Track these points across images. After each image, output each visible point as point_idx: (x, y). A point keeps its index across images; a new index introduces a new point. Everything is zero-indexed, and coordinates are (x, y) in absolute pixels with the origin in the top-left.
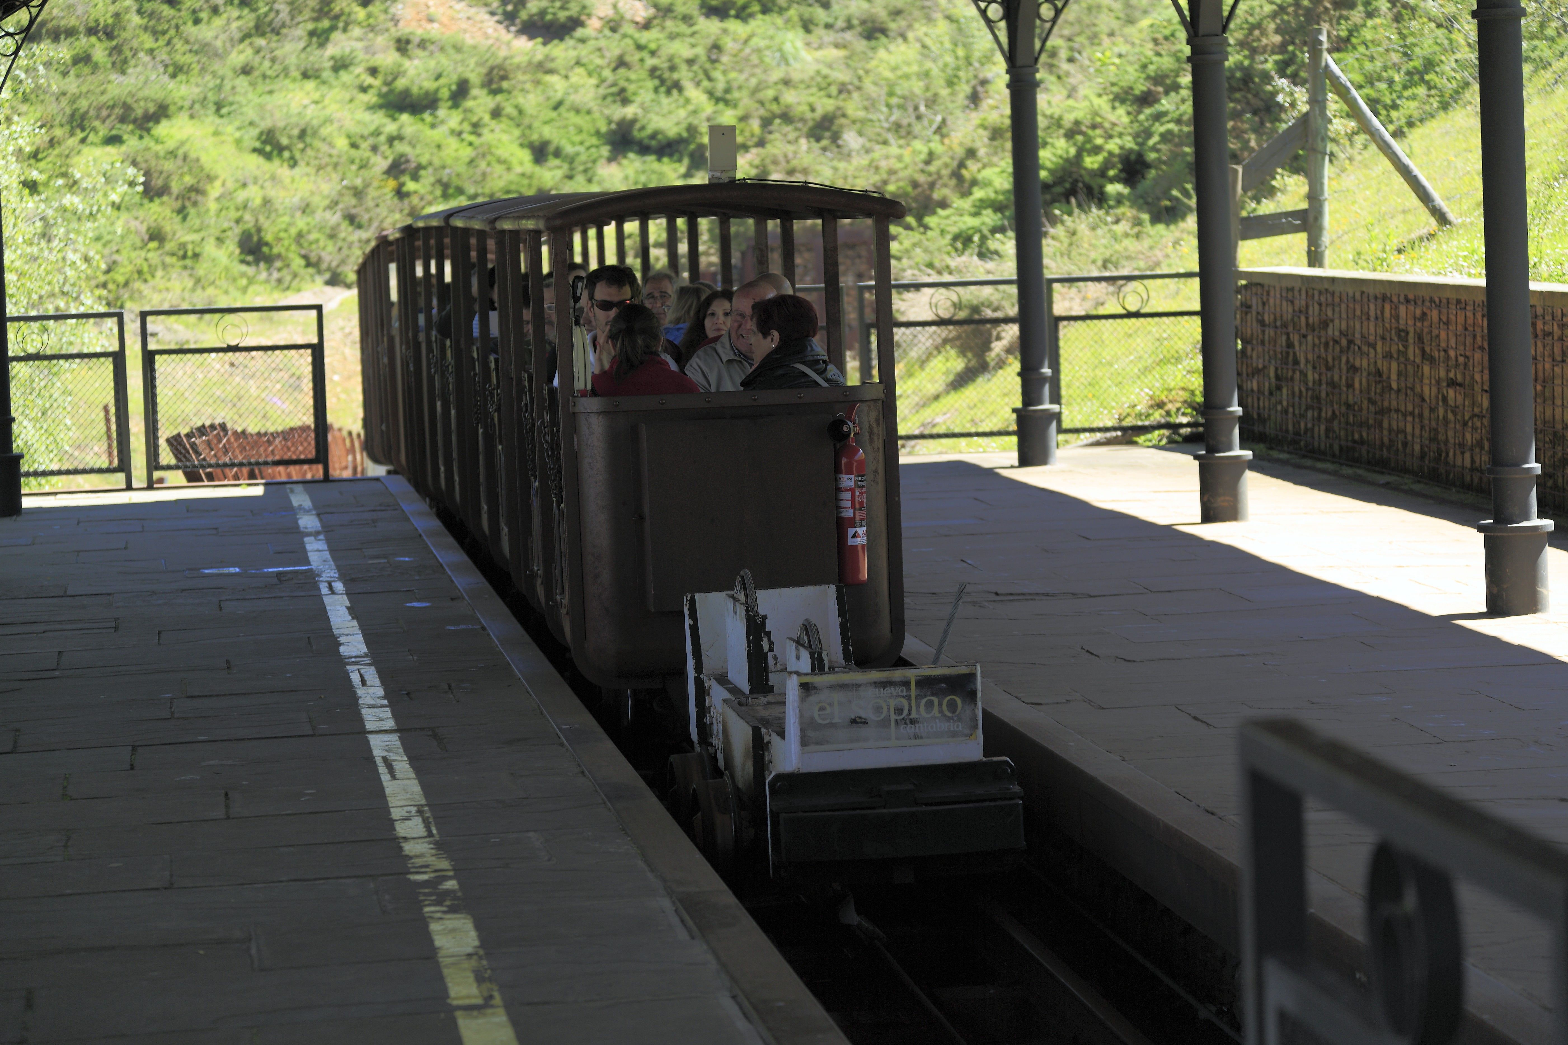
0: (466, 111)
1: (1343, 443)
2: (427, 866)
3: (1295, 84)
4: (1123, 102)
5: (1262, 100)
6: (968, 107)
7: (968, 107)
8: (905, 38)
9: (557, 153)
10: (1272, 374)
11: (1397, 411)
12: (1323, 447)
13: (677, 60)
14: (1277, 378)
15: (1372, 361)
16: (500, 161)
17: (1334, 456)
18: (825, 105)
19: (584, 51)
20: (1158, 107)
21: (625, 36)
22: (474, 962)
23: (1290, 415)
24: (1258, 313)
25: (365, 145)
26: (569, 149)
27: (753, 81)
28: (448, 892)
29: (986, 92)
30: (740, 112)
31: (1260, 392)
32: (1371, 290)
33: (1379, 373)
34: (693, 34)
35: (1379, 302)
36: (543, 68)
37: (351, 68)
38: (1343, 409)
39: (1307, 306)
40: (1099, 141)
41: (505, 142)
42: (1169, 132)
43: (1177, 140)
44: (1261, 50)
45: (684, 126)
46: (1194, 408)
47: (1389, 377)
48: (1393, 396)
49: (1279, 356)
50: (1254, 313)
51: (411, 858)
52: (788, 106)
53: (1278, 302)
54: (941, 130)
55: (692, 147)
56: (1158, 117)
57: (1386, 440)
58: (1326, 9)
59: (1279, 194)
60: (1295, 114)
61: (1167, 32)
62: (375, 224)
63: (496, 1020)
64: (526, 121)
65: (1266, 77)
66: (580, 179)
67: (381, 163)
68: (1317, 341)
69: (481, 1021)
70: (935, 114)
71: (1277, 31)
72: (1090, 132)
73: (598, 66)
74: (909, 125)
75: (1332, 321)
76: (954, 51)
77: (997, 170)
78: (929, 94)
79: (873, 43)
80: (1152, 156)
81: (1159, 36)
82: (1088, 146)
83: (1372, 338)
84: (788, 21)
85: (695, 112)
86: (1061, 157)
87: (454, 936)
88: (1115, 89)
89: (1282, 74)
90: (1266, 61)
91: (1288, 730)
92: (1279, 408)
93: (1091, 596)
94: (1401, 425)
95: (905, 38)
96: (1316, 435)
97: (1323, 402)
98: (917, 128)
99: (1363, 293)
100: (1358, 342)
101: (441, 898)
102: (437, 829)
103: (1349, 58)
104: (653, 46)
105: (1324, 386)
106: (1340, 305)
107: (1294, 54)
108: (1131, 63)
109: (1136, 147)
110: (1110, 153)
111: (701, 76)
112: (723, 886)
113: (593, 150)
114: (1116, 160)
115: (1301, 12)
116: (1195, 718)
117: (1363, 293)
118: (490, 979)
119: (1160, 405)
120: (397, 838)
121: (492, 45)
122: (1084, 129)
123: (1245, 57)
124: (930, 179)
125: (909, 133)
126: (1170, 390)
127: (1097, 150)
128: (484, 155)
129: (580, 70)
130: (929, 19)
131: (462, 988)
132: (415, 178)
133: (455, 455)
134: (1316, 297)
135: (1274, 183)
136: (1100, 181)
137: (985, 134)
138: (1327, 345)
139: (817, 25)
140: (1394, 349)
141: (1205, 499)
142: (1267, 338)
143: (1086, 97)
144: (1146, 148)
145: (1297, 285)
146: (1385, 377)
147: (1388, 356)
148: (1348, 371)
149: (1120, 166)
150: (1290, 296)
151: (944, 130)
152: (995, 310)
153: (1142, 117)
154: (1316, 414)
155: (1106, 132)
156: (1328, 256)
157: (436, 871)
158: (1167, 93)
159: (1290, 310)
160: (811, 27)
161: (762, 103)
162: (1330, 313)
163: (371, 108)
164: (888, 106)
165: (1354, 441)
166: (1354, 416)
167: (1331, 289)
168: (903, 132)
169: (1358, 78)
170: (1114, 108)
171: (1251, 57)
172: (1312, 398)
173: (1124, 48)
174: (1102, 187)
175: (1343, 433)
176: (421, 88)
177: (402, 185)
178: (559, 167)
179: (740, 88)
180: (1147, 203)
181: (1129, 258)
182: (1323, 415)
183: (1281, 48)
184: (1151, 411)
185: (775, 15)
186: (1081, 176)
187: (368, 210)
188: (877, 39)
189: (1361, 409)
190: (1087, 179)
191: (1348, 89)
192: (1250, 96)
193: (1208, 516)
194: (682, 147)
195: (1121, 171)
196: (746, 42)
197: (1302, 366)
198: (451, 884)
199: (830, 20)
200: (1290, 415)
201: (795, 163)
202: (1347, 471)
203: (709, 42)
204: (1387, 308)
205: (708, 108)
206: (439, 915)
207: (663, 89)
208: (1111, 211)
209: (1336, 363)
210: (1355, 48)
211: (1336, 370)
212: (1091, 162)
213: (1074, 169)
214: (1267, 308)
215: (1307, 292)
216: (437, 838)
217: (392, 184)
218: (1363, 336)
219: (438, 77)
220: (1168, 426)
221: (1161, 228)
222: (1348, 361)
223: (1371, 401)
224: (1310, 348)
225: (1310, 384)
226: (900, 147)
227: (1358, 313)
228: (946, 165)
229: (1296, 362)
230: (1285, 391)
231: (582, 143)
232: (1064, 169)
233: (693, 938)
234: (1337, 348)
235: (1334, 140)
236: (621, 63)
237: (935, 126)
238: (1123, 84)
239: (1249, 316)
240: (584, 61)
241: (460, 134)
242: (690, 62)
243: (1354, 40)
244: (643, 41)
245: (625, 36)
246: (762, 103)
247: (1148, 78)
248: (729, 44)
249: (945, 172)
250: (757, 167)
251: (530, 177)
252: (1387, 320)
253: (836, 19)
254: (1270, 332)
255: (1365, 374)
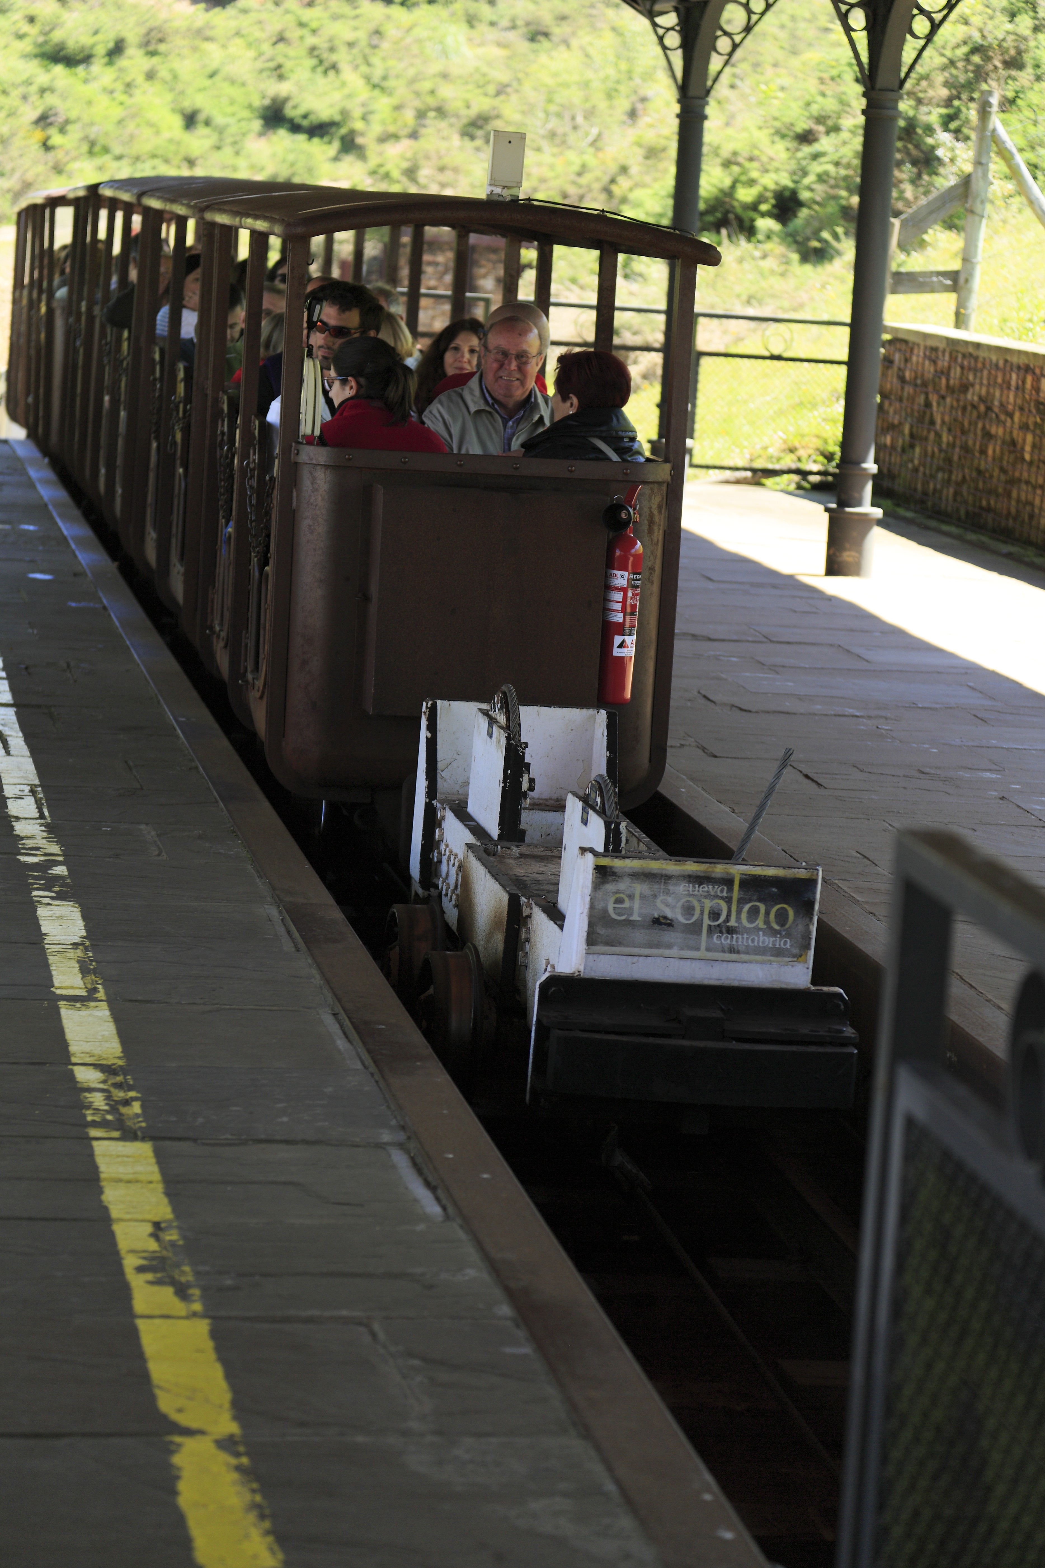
0: (121, 70)
1: (970, 508)
2: (38, 849)
3: (958, 140)
4: (783, 136)
5: (922, 151)
6: (624, 123)
7: (624, 123)
8: (568, 46)
9: (207, 123)
10: (907, 430)
11: (1028, 482)
12: (949, 509)
13: (336, 42)
14: (912, 435)
15: (1008, 430)
16: (151, 125)
17: (959, 519)
18: (481, 104)
19: (244, 22)
20: (816, 147)
21: (287, 12)
22: (79, 953)
23: (920, 475)
24: (899, 369)
25: (16, 93)
26: (219, 119)
27: (411, 72)
28: (57, 878)
29: (645, 109)
30: (394, 101)
31: (893, 447)
32: (1015, 360)
33: (1013, 443)
34: (357, 17)
35: (1022, 373)
36: (202, 35)
37: (9, 14)
38: (974, 474)
39: (949, 368)
40: (754, 174)
41: (159, 109)
42: (826, 173)
43: (832, 182)
44: (926, 101)
45: (337, 108)
46: (826, 457)
47: (1023, 449)
48: (1025, 467)
49: (916, 414)
50: (895, 369)
51: (22, 838)
52: (443, 100)
53: (921, 360)
54: (596, 144)
55: (343, 131)
56: (816, 156)
57: (1013, 510)
58: (996, 67)
59: (929, 248)
60: (954, 169)
61: (834, 72)
62: (17, 175)
63: (99, 1013)
64: (180, 87)
65: (929, 130)
66: (228, 151)
67: (30, 113)
68: (955, 404)
69: (84, 1013)
70: (592, 126)
71: (946, 84)
72: (747, 165)
73: (257, 40)
74: (565, 135)
75: (973, 385)
76: (616, 64)
77: (649, 191)
78: (588, 105)
79: (535, 46)
80: (805, 195)
81: (826, 76)
82: (744, 178)
83: (1010, 407)
84: (453, 14)
85: (350, 96)
86: (715, 186)
87: (61, 924)
88: (777, 124)
89: (946, 129)
90: (930, 113)
91: (946, 844)
92: (910, 466)
93: (710, 639)
94: (1030, 497)
95: (568, 46)
96: (944, 498)
97: (954, 465)
98: (572, 138)
99: (1006, 361)
100: (996, 410)
101: (50, 883)
102: (49, 812)
103: (1013, 117)
104: (314, 25)
105: (957, 450)
106: (982, 371)
107: (959, 111)
108: (796, 99)
109: (791, 185)
110: (766, 189)
111: (360, 61)
112: (331, 901)
113: (243, 123)
114: (769, 195)
115: (971, 68)
116: (807, 776)
117: (1006, 361)
118: (95, 972)
119: (792, 450)
120: (10, 816)
121: (153, 6)
122: (740, 159)
123: (910, 106)
124: (581, 191)
125: (564, 142)
126: (803, 436)
127: (752, 183)
128: (133, 116)
129: (238, 41)
130: (594, 28)
131: (66, 977)
132: (62, 130)
133: (119, 462)
134: (960, 360)
135: (925, 237)
136: (752, 214)
137: (640, 152)
138: (964, 409)
139: (481, 21)
140: (1031, 421)
141: (831, 552)
142: (905, 394)
143: (745, 129)
144: (800, 185)
145: (942, 345)
146: (1019, 447)
147: (1024, 427)
148: (983, 437)
149: (773, 201)
150: (933, 356)
151: (599, 144)
152: (635, 333)
153: (800, 155)
154: (946, 476)
155: (762, 165)
156: (974, 319)
157: (46, 855)
158: (828, 133)
159: (932, 369)
160: (475, 23)
161: (417, 94)
162: (971, 377)
163: (26, 56)
164: (547, 113)
165: (981, 508)
166: (984, 483)
167: (975, 353)
168: (558, 140)
169: (1022, 143)
170: (773, 142)
171: (916, 108)
172: (944, 460)
173: (786, 81)
174: (753, 220)
175: (971, 498)
176: (77, 42)
177: (48, 138)
178: (208, 137)
179: (397, 77)
180: (796, 242)
181: (773, 296)
182: (953, 478)
183: (948, 103)
184: (782, 455)
185: (441, 7)
186: (733, 207)
187: (12, 159)
188: (539, 41)
189: (991, 477)
190: (739, 210)
191: (1012, 154)
192: (910, 146)
193: (833, 568)
194: (333, 129)
195: (774, 206)
196: (409, 30)
197: (938, 427)
198: (61, 870)
199: (494, 18)
200: (920, 475)
201: (446, 160)
202: (971, 536)
203: (372, 26)
204: (1029, 380)
205: (363, 92)
206: (47, 900)
207: (320, 69)
208: (760, 246)
209: (972, 428)
210: (1020, 110)
211: (972, 435)
212: (745, 195)
213: (727, 200)
214: (909, 365)
215: (951, 354)
216: (49, 820)
217: (39, 135)
218: (1002, 405)
219: (96, 33)
220: (798, 472)
221: (808, 268)
222: (984, 428)
223: (1003, 470)
224: (947, 410)
225: (944, 446)
226: (554, 155)
227: (1000, 380)
228: (598, 179)
229: (932, 422)
230: (918, 450)
231: (234, 115)
232: (717, 199)
233: (298, 950)
234: (975, 413)
235: (992, 202)
236: (281, 39)
237: (591, 138)
238: (787, 120)
239: (890, 372)
240: (244, 32)
241: (112, 92)
242: (351, 45)
243: (1019, 102)
244: (304, 19)
245: (287, 12)
246: (417, 94)
247: (811, 117)
248: (391, 31)
249: (597, 186)
250: (408, 160)
251: (178, 143)
252: (1027, 391)
253: (502, 17)
254: (909, 390)
255: (999, 442)
